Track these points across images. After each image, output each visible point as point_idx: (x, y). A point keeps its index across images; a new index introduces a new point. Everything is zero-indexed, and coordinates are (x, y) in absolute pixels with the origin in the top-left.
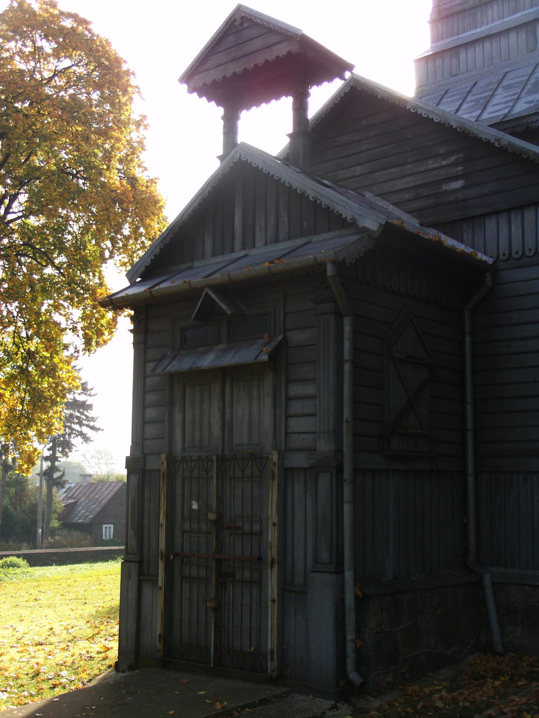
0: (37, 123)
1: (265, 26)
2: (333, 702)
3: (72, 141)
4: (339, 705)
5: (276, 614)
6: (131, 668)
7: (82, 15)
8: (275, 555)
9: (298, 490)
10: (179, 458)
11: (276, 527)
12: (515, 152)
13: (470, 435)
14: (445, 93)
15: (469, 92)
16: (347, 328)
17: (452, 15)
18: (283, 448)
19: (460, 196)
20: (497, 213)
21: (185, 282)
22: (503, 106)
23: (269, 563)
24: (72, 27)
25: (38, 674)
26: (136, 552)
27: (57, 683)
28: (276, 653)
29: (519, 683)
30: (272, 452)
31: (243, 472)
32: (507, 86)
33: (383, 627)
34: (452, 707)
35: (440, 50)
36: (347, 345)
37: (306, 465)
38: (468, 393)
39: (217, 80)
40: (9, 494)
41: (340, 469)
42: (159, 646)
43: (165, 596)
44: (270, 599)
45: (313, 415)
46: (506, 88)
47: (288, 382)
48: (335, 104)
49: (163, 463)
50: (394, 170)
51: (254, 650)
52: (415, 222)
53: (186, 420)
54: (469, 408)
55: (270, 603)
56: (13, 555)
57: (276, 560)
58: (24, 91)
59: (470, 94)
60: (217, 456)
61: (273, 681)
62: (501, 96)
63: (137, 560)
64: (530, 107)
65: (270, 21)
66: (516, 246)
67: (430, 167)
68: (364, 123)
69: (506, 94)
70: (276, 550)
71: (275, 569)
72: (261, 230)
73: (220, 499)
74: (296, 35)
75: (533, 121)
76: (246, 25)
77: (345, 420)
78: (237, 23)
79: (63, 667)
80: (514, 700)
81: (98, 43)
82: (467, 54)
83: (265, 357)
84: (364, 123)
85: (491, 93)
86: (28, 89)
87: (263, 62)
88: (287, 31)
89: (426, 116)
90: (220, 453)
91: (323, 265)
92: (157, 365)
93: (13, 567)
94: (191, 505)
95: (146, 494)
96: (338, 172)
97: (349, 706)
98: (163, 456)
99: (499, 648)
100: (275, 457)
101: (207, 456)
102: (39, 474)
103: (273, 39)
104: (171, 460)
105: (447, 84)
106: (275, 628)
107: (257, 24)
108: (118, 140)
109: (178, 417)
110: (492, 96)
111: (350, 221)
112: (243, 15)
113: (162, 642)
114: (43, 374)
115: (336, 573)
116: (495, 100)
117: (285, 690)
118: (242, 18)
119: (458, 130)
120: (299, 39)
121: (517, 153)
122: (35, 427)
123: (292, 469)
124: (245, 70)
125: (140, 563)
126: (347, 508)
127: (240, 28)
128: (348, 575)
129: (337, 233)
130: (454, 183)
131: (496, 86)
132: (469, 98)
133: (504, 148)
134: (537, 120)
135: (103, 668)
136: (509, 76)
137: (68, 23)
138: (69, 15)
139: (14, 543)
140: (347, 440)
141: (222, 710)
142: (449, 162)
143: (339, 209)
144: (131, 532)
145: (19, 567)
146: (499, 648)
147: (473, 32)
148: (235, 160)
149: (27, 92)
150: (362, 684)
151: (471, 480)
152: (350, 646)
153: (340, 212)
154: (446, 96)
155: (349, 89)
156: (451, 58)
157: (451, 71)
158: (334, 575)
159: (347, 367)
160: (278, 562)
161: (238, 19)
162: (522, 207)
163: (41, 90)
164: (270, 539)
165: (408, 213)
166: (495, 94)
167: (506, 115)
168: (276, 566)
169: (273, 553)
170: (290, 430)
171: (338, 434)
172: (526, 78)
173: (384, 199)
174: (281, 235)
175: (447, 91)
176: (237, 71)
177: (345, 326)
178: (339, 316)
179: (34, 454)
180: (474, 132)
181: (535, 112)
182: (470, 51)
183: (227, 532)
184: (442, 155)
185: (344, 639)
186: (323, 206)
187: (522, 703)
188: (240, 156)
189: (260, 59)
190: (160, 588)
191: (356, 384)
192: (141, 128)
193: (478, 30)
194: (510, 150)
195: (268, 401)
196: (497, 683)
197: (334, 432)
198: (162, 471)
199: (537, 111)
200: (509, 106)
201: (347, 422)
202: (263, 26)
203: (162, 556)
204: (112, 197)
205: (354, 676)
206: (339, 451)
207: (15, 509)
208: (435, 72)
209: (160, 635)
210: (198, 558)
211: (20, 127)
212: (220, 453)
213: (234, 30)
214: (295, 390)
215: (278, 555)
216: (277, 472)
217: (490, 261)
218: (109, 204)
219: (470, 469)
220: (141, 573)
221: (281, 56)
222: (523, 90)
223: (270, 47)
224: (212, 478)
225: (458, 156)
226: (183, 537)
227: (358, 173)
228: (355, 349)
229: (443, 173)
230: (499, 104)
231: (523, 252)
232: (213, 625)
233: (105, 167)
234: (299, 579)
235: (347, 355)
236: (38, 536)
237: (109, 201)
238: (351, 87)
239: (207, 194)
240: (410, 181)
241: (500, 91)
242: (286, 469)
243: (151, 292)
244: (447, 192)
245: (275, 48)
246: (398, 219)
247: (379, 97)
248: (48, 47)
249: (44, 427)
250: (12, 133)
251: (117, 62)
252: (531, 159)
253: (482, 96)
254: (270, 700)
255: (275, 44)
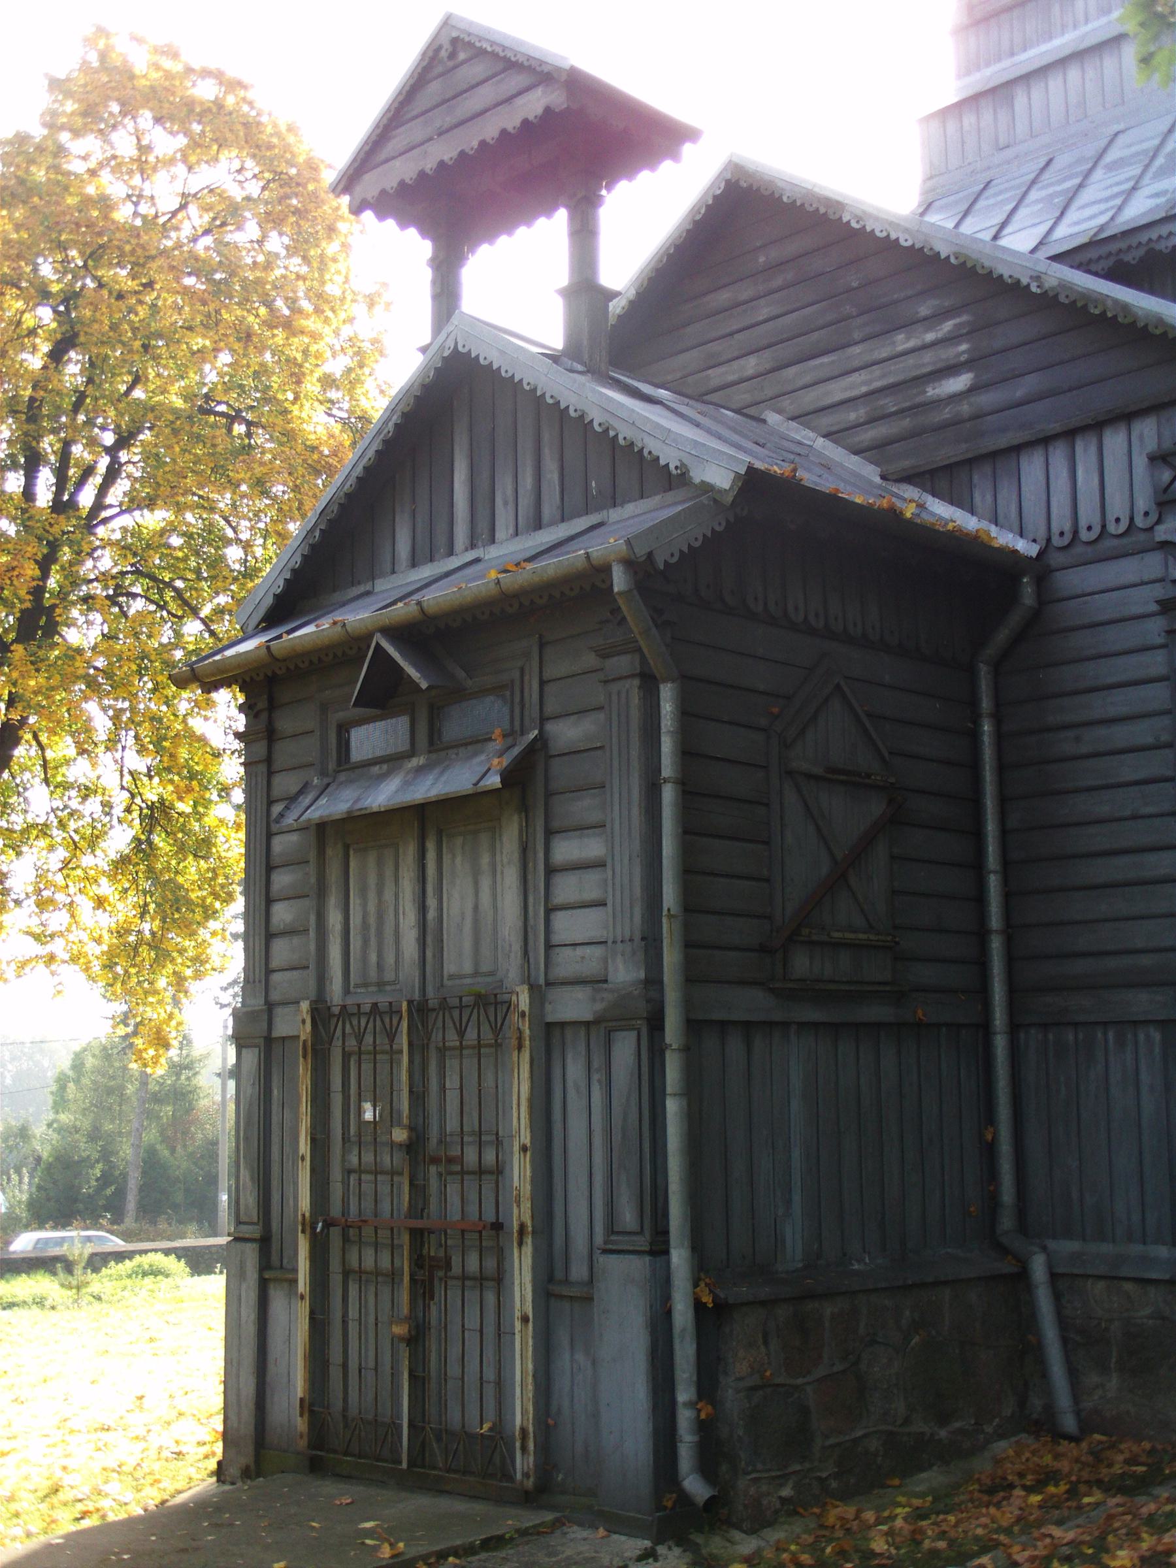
0: (139, 308)
1: (509, 59)
2: (647, 1543)
3: (215, 342)
4: (661, 1550)
5: (530, 1349)
6: (246, 1474)
7: (231, 73)
8: (528, 1220)
9: (575, 1070)
10: (336, 1010)
11: (528, 1154)
12: (1075, 302)
13: (996, 944)
14: (984, 189)
15: (1034, 182)
16: (667, 708)
17: (996, 14)
18: (542, 981)
19: (965, 408)
20: (1045, 441)
21: (335, 623)
22: (1103, 206)
23: (515, 1235)
24: (217, 98)
25: (57, 1490)
26: (255, 1219)
27: (91, 1508)
28: (531, 1435)
29: (1086, 1500)
30: (518, 989)
31: (461, 1033)
32: (1115, 162)
33: (768, 1374)
34: (903, 1551)
35: (970, 92)
36: (667, 745)
37: (588, 1017)
38: (990, 849)
39: (408, 181)
40: (159, 1118)
41: (656, 1023)
42: (301, 1424)
43: (312, 1313)
44: (517, 1314)
45: (602, 904)
46: (1110, 167)
47: (550, 833)
48: (696, 223)
49: (304, 1022)
50: (825, 359)
51: (490, 1429)
52: (872, 473)
53: (352, 926)
54: (994, 883)
55: (518, 1325)
56: (156, 1251)
57: (530, 1229)
58: (110, 241)
59: (1036, 186)
60: (410, 1002)
61: (531, 1498)
62: (1100, 187)
63: (257, 1235)
64: (1157, 206)
65: (506, 44)
66: (1088, 514)
67: (900, 348)
68: (762, 259)
69: (1110, 182)
70: (529, 1205)
71: (528, 1249)
72: (506, 503)
73: (418, 1097)
74: (559, 69)
75: (1160, 237)
76: (462, 56)
77: (665, 912)
78: (444, 54)
79: (115, 1475)
80: (1050, 1536)
81: (269, 130)
82: (1030, 99)
83: (494, 781)
84: (762, 259)
85: (1077, 181)
86: (118, 235)
87: (496, 134)
88: (542, 63)
89: (884, 234)
90: (417, 996)
91: (604, 570)
92: (287, 808)
93: (156, 1276)
94: (360, 1112)
95: (275, 1092)
96: (710, 371)
97: (684, 1551)
98: (305, 1006)
99: (1069, 1423)
100: (523, 1000)
101: (390, 1003)
102: (219, 1075)
103: (516, 81)
104: (321, 1014)
105: (989, 168)
106: (530, 1379)
107: (482, 52)
108: (315, 336)
109: (334, 919)
110: (1081, 186)
111: (674, 472)
112: (454, 34)
113: (306, 1415)
114: (182, 850)
115: (652, 1253)
116: (1086, 196)
117: (549, 1516)
118: (455, 41)
119: (953, 260)
120: (564, 78)
121: (1079, 304)
122: (170, 966)
123: (563, 1025)
124: (462, 154)
125: (265, 1242)
126: (673, 1107)
127: (451, 64)
128: (679, 1258)
129: (656, 500)
130: (952, 381)
131: (1089, 165)
132: (1034, 195)
133: (1051, 294)
134: (1170, 234)
135: (196, 1476)
136: (1121, 140)
137: (206, 91)
138: (206, 73)
139: (170, 1224)
140: (671, 957)
141: (391, 1561)
142: (940, 335)
143: (653, 446)
144: (245, 1174)
145: (167, 1276)
146: (1069, 1423)
147: (1044, 48)
148: (446, 354)
149: (116, 243)
150: (711, 1503)
151: (1000, 1043)
152: (685, 1418)
153: (655, 453)
154: (987, 193)
155: (722, 186)
156: (995, 111)
157: (997, 140)
158: (647, 1259)
159: (668, 794)
160: (533, 1232)
161: (447, 45)
162: (1097, 426)
163: (146, 238)
164: (516, 1183)
165: (856, 453)
166: (1140, 185)
167: (1102, 228)
168: (529, 1240)
169: (521, 1213)
170: (556, 939)
171: (651, 943)
172: (1156, 142)
173: (807, 426)
174: (548, 511)
175: (989, 183)
176: (446, 158)
177: (662, 703)
178: (649, 682)
179: (168, 1025)
180: (987, 264)
181: (1164, 215)
182: (1037, 92)
183: (433, 1169)
184: (925, 319)
185: (673, 1402)
186: (622, 442)
187: (1065, 1541)
188: (456, 343)
189: (489, 130)
190: (302, 1297)
191: (689, 831)
192: (378, 309)
193: (1057, 42)
194: (1062, 299)
195: (510, 877)
196: (1035, 1499)
197: (643, 939)
198: (303, 1038)
199: (1170, 213)
200: (1112, 208)
201: (670, 916)
202: (494, 55)
203: (303, 1224)
204: (310, 462)
205: (695, 1487)
206: (653, 981)
207: (173, 1150)
208: (963, 143)
209: (302, 1400)
210: (376, 1228)
211: (103, 318)
212: (417, 996)
213: (439, 69)
214: (566, 850)
215: (532, 1217)
216: (527, 1032)
217: (1023, 546)
218: (303, 476)
219: (999, 1018)
220: (265, 1264)
221: (531, 118)
222: (1147, 167)
223: (509, 100)
224: (401, 1052)
225: (957, 320)
226: (346, 1184)
227: (750, 372)
228: (687, 753)
229: (928, 361)
230: (1094, 203)
231: (1104, 526)
232: (406, 1375)
233: (290, 396)
234: (579, 1271)
235: (668, 768)
236: (220, 1208)
237: (301, 470)
238: (728, 182)
239: (391, 430)
240: (859, 384)
241: (1098, 174)
242: (549, 1025)
243: (268, 648)
244: (938, 403)
245: (520, 101)
246: (827, 466)
247: (785, 199)
248: (166, 143)
249: (188, 967)
250: (86, 333)
251: (311, 168)
252: (1109, 315)
253: (1059, 188)
254: (512, 1539)
255: (520, 93)
